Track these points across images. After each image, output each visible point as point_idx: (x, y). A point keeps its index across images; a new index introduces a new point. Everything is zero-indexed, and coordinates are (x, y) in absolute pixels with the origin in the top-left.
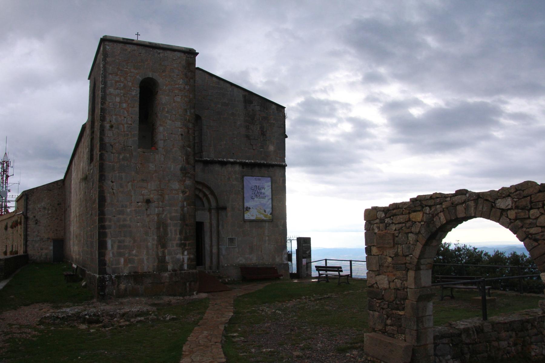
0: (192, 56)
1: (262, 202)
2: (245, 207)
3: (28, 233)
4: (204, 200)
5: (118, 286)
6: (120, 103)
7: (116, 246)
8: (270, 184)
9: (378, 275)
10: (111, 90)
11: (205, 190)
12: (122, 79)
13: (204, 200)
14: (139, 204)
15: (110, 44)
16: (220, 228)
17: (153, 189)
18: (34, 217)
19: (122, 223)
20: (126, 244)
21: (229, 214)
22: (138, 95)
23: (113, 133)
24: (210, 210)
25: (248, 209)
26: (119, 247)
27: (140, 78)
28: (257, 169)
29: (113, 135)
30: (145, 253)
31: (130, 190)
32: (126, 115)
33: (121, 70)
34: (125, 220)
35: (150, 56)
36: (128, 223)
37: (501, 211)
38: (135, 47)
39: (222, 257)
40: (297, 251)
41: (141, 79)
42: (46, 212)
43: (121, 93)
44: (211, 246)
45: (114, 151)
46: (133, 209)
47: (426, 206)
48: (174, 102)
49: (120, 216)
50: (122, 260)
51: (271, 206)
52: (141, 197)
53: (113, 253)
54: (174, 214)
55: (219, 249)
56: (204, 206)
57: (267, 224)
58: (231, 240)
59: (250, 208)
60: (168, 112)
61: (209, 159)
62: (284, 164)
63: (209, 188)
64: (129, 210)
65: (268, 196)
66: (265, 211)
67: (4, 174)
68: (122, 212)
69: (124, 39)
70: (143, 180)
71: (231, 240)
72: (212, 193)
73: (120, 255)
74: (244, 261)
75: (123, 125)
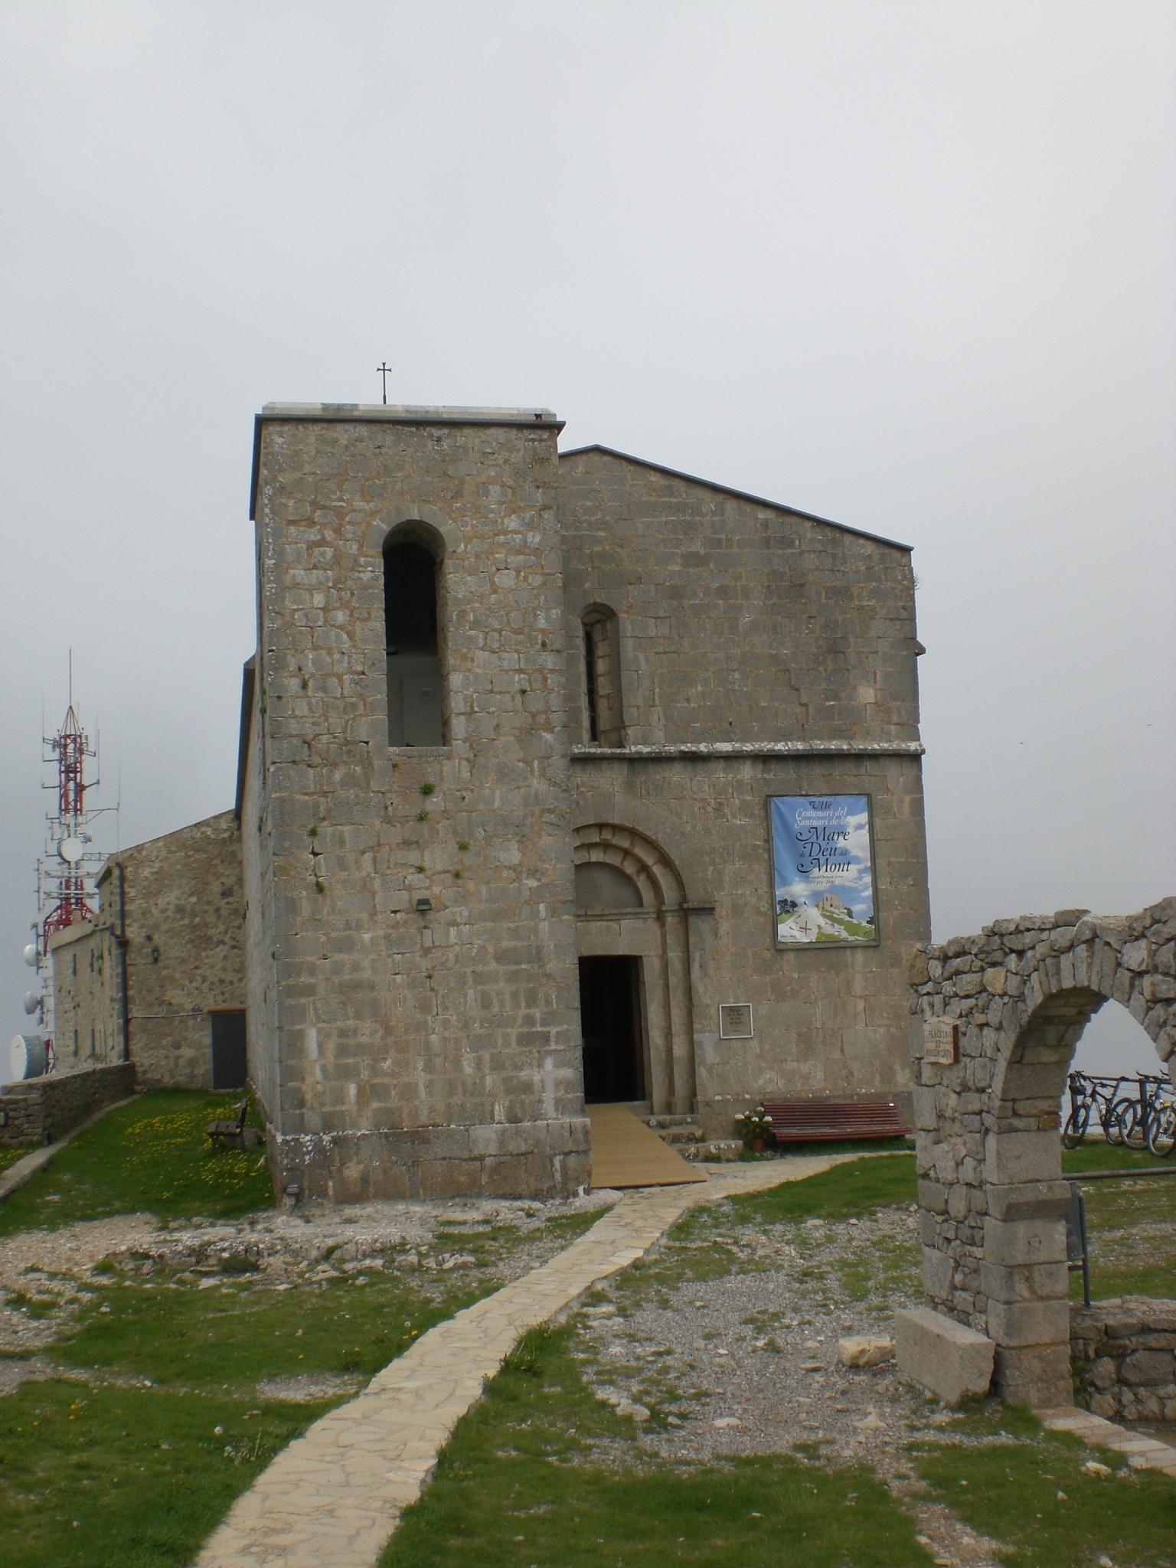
0: (545, 435)
1: (837, 882)
3: (131, 993)
4: (642, 882)
5: (340, 1171)
6: (325, 609)
7: (331, 1047)
8: (864, 817)
9: (937, 1142)
10: (298, 573)
11: (640, 851)
12: (329, 535)
13: (642, 882)
14: (399, 915)
15: (286, 428)
17: (439, 867)
18: (149, 938)
19: (347, 977)
20: (363, 1039)
21: (724, 927)
22: (382, 581)
23: (309, 704)
24: (660, 917)
25: (790, 906)
26: (342, 1051)
27: (383, 526)
28: (818, 770)
30: (420, 1065)
31: (369, 874)
33: (324, 507)
34: (356, 968)
35: (410, 451)
36: (366, 975)
37: (1130, 974)
38: (363, 430)
39: (702, 1071)
41: (386, 528)
42: (186, 921)
43: (327, 579)
44: (668, 1035)
45: (317, 760)
46: (381, 933)
47: (1012, 951)
48: (495, 592)
49: (343, 956)
50: (352, 1089)
51: (869, 892)
52: (404, 895)
53: (324, 1069)
54: (505, 944)
55: (691, 1044)
56: (641, 905)
57: (860, 956)
58: (735, 1015)
60: (476, 625)
61: (646, 750)
62: (913, 746)
63: (652, 845)
64: (367, 937)
65: (857, 860)
66: (850, 914)
67: (68, 780)
68: (346, 945)
69: (326, 407)
70: (407, 843)
71: (735, 1015)
72: (665, 861)
73: (345, 1073)
74: (781, 1082)
75: (340, 680)
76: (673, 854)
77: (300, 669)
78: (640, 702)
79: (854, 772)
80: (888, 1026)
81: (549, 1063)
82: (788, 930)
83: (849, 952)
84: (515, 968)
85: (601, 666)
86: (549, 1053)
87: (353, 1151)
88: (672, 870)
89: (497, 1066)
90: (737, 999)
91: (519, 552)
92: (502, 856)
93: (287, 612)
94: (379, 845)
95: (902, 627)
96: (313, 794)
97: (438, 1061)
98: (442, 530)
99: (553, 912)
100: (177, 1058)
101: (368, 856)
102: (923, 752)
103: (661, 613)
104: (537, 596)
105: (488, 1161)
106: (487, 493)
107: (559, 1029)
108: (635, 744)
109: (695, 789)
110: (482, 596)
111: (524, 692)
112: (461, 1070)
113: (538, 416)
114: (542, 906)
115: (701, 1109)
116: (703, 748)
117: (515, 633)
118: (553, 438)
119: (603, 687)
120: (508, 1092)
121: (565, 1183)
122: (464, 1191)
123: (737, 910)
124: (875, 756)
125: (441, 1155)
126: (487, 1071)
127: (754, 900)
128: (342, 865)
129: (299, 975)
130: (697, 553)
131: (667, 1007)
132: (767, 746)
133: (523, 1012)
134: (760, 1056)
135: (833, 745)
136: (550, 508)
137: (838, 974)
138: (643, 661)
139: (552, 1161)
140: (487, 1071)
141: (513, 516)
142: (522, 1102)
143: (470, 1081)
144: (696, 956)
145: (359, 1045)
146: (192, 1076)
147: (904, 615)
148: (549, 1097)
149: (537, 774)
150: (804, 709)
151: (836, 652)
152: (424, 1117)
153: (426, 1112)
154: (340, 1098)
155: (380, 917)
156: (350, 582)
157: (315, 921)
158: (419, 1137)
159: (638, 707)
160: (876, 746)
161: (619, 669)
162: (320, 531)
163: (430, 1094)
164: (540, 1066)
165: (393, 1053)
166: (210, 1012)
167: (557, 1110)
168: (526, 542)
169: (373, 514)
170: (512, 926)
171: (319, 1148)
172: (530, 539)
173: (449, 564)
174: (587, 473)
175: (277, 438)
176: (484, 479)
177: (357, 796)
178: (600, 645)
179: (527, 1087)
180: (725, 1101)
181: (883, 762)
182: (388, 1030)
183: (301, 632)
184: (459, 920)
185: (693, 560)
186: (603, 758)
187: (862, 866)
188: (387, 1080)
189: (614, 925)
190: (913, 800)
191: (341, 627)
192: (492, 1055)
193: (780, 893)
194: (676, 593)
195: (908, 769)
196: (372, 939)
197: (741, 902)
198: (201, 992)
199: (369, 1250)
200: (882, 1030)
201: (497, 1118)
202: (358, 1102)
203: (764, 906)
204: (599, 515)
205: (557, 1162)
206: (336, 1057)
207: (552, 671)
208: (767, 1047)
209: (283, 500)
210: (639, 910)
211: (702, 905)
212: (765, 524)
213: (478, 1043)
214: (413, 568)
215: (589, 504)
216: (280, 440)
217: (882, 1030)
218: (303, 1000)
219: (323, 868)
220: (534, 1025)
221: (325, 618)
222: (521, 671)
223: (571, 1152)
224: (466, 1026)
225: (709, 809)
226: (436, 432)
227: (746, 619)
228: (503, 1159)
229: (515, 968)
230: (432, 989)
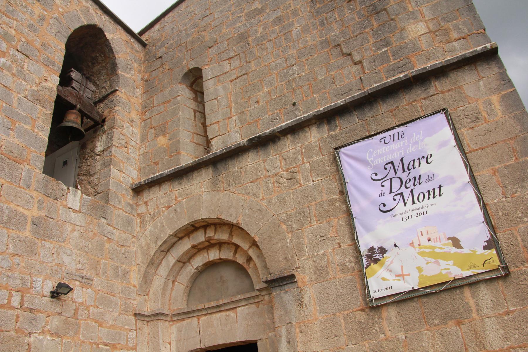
2: (364, 250)
8: (447, 132)
21: (310, 294)
25: (376, 255)
41: (86, 23)
57: (485, 294)
59: (383, 251)
65: (452, 180)
66: (456, 242)
78: (220, 118)
79: (423, 96)
82: (382, 282)
83: (467, 292)
109: (268, 168)
123: (320, 272)
127: (338, 258)
137: (459, 324)
150: (359, 66)
151: (377, 13)
187: (459, 184)
189: (231, 313)
190: (504, 97)
193: (366, 242)
195: (487, 73)
197: (324, 263)
203: (349, 260)
225: (283, 181)
227: (297, 28)
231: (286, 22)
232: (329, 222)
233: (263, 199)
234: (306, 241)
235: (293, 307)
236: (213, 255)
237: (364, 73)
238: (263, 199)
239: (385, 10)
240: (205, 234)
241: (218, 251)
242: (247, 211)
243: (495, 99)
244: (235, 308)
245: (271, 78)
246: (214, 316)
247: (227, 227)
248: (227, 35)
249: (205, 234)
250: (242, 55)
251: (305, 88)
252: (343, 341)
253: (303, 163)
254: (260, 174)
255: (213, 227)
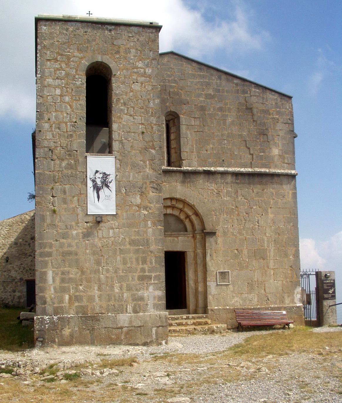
4: (187, 222)
5: (61, 331)
6: (61, 96)
7: (58, 279)
10: (50, 81)
12: (63, 65)
15: (47, 23)
16: (208, 258)
20: (71, 276)
21: (220, 240)
23: (53, 134)
24: (194, 237)
26: (63, 281)
27: (86, 63)
28: (257, 179)
29: (53, 136)
30: (96, 288)
31: (76, 207)
32: (69, 110)
33: (62, 55)
34: (70, 245)
35: (98, 34)
36: (73, 249)
39: (210, 298)
40: (317, 289)
41: (87, 64)
43: (62, 83)
44: (196, 282)
45: (55, 157)
48: (132, 91)
49: (64, 241)
50: (67, 297)
53: (55, 288)
58: (223, 275)
61: (190, 169)
62: (293, 172)
63: (192, 207)
64: (74, 232)
68: (65, 236)
72: (197, 214)
73: (64, 290)
75: (66, 123)
76: (200, 211)
77: (49, 119)
80: (283, 281)
81: (151, 288)
84: (137, 248)
85: (172, 137)
86: (152, 284)
87: (66, 323)
88: (199, 217)
89: (129, 289)
90: (224, 269)
91: (142, 76)
92: (133, 200)
93: (45, 96)
94: (81, 194)
95: (289, 126)
96: (53, 171)
97: (103, 286)
98: (111, 66)
99: (154, 224)
100: (14, 296)
101: (76, 198)
102: (297, 174)
103: (196, 116)
104: (149, 94)
105: (125, 329)
106: (130, 52)
107: (155, 274)
108: (186, 166)
110: (126, 93)
111: (143, 133)
112: (114, 291)
113: (151, 23)
114: (149, 222)
115: (210, 312)
116: (212, 169)
117: (141, 108)
118: (155, 40)
119: (173, 145)
120: (133, 300)
121: (157, 339)
122: (115, 342)
123: (225, 233)
124: (278, 175)
125: (104, 326)
126: (125, 291)
128: (65, 201)
129: (45, 248)
130: (210, 94)
131: (196, 271)
132: (237, 169)
133: (141, 266)
134: (233, 291)
135: (263, 170)
136: (156, 59)
138: (189, 135)
139: (151, 330)
140: (125, 291)
141: (140, 62)
142: (139, 305)
143: (117, 295)
144: (208, 252)
145: (70, 279)
146: (19, 302)
147: (289, 122)
148: (151, 303)
149: (148, 166)
150: (251, 156)
152: (97, 310)
153: (98, 308)
154: (61, 301)
155: (80, 225)
156: (72, 85)
157: (53, 225)
158: (95, 318)
159: (187, 152)
160: (279, 171)
161: (180, 137)
162: (60, 64)
163: (100, 300)
164: (147, 289)
165: (84, 282)
166: (26, 280)
167: (154, 308)
168: (145, 72)
169: (81, 58)
170: (137, 230)
171: (52, 322)
172: (147, 71)
173: (113, 80)
174: (168, 61)
175: (44, 28)
176: (128, 46)
177: (72, 173)
178: (172, 128)
179: (142, 299)
180: (219, 309)
181: (281, 177)
182: (83, 272)
183: (50, 105)
184: (114, 227)
185: (209, 97)
186: (173, 171)
188: (81, 294)
189: (176, 239)
191: (67, 103)
192: (127, 285)
194: (202, 109)
196: (77, 233)
198: (23, 273)
199: (69, 366)
200: (280, 282)
201: (128, 311)
202: (69, 303)
204: (173, 78)
205: (154, 330)
206: (61, 283)
207: (155, 124)
208: (236, 288)
209: (45, 51)
210: (186, 233)
211: (210, 231)
212: (237, 85)
213: (121, 279)
214: (98, 85)
215: (168, 73)
216: (45, 28)
217: (280, 282)
218: (46, 259)
219: (57, 203)
220: (145, 272)
221: (61, 99)
222: (142, 124)
223: (160, 326)
224: (116, 272)
225: (215, 193)
226: (109, 27)
227: (229, 120)
228: (131, 328)
229: (137, 248)
230: (102, 256)
231: (224, 113)
232: (230, 216)
233: (206, 198)
234: (221, 220)
235: (213, 243)
236: (169, 211)
237: (253, 160)
238: (206, 198)
239: (267, 135)
240: (171, 202)
241: (172, 211)
242: (198, 201)
243: (290, 192)
244: (178, 237)
245: (214, 141)
246: (167, 238)
247: (182, 203)
248: (194, 102)
249: (171, 202)
250: (201, 119)
251: (229, 155)
252: (229, 258)
253: (224, 189)
254: (205, 186)
255: (175, 200)
